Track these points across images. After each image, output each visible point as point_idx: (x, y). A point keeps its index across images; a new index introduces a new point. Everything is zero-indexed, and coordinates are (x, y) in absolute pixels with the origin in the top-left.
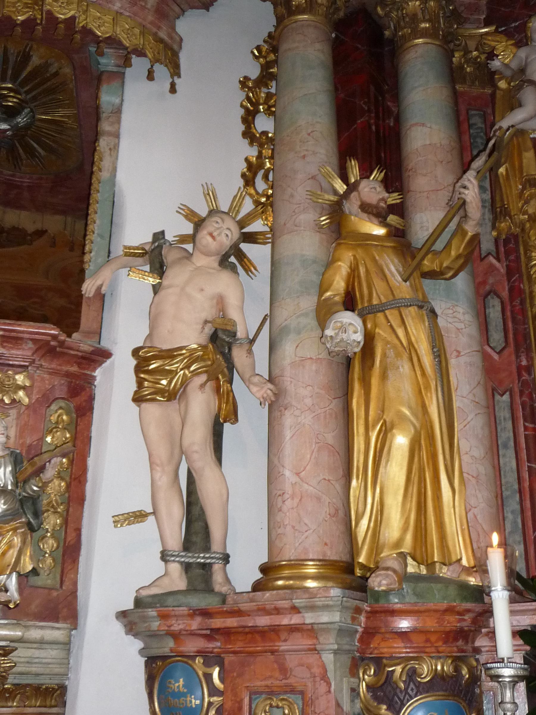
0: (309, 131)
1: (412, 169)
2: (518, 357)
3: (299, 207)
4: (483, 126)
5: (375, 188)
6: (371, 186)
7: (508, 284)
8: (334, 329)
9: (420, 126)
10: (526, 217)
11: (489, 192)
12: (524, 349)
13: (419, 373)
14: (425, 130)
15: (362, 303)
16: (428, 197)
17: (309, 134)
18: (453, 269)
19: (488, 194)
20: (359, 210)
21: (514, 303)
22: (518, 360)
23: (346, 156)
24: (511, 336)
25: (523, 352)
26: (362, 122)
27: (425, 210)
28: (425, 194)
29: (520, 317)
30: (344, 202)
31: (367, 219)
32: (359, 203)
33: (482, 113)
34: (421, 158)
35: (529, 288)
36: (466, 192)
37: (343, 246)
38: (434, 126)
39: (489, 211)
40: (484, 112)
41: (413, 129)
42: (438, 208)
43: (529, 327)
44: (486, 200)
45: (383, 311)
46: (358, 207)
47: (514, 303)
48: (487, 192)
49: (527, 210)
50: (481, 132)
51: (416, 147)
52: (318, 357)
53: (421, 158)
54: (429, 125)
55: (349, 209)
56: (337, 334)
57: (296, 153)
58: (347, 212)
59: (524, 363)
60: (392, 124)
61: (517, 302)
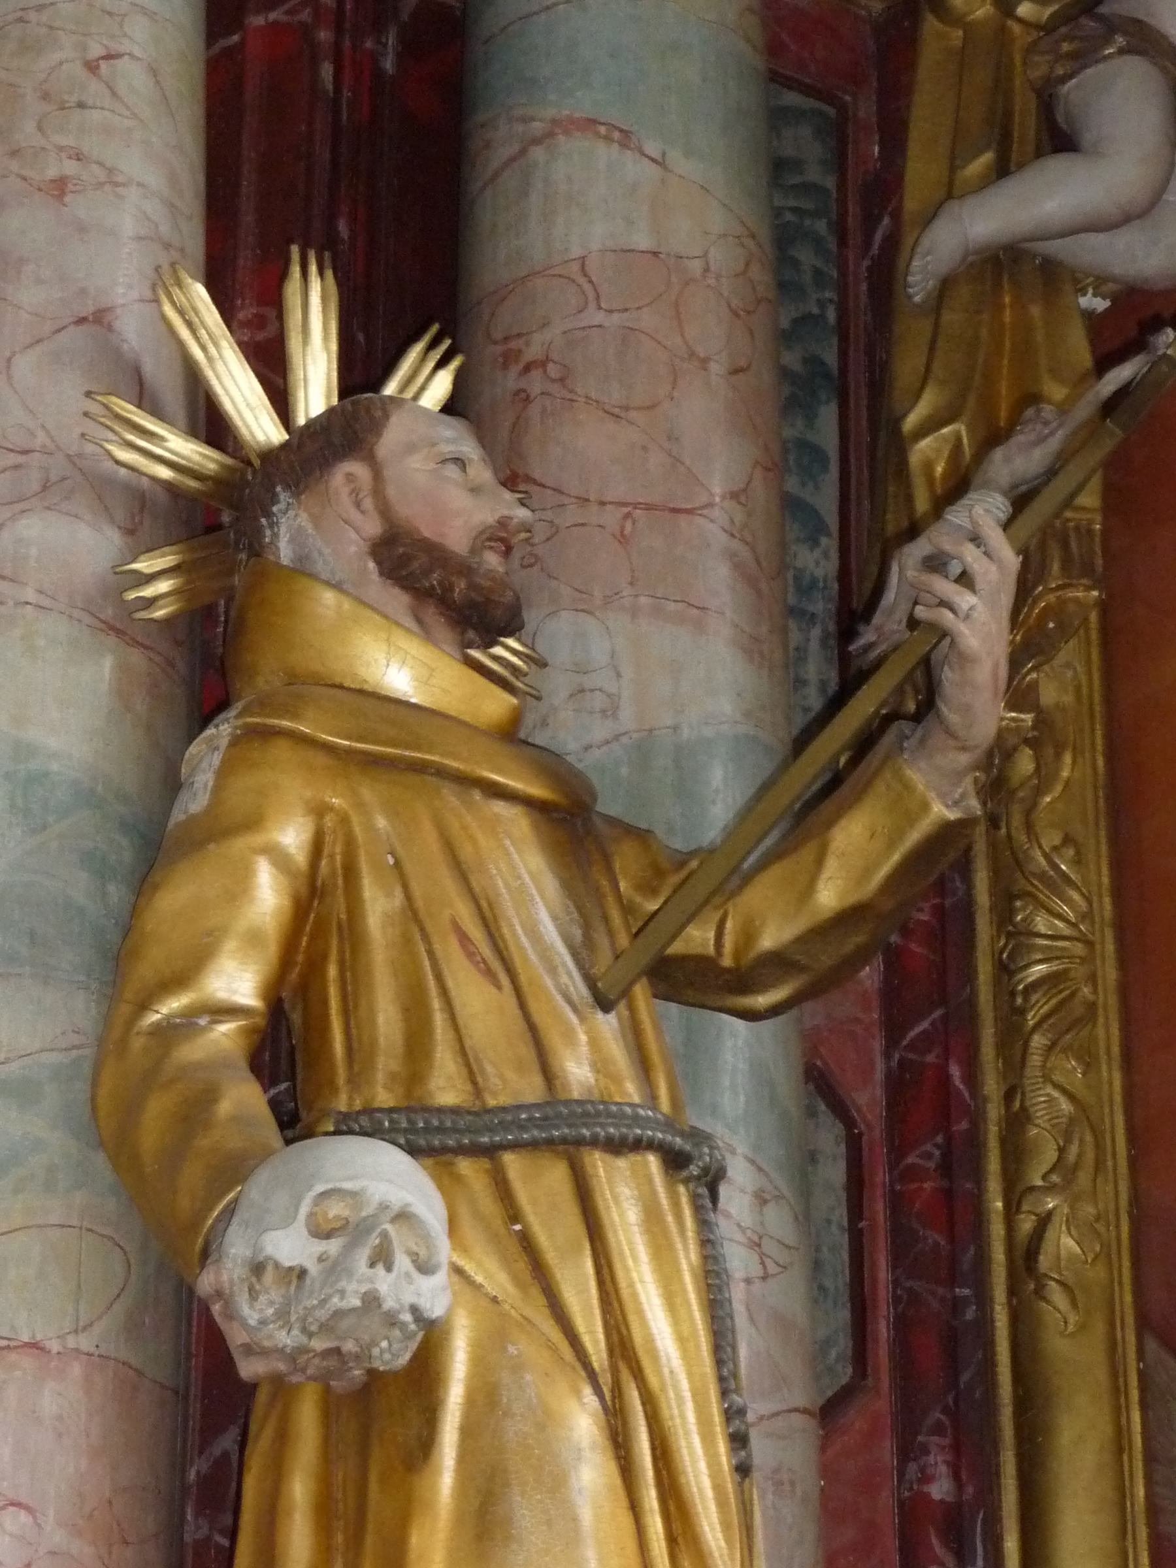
0: (96, 51)
1: (543, 364)
2: (908, 1451)
3: (17, 467)
4: (830, 183)
5: (460, 462)
6: (447, 449)
7: (887, 1055)
8: (321, 1233)
9: (608, 139)
10: (1028, 718)
11: (830, 543)
12: (945, 1410)
13: (656, 1525)
14: (634, 168)
15: (359, 1078)
16: (623, 539)
17: (92, 67)
18: (801, 969)
19: (826, 555)
20: (371, 565)
21: (910, 1159)
22: (912, 1468)
23: (290, 241)
24: (883, 1330)
25: (938, 1429)
26: (274, 25)
27: (607, 601)
28: (611, 517)
29: (935, 1238)
30: (284, 496)
31: (410, 623)
32: (373, 527)
33: (831, 111)
34: (599, 318)
35: (1009, 1096)
36: (966, 600)
37: (281, 750)
38: (675, 157)
39: (824, 642)
40: (842, 109)
41: (572, 146)
42: (672, 607)
43: (983, 1299)
44: (814, 581)
45: (491, 1152)
46: (365, 547)
47: (910, 1159)
48: (824, 541)
49: (1034, 686)
50: (816, 214)
51: (576, 252)
52: (71, 1342)
53: (599, 318)
54: (652, 147)
55: (298, 537)
56: (334, 1268)
57: (14, 153)
58: (285, 552)
59: (940, 1489)
60: (388, 64)
61: (928, 1156)
